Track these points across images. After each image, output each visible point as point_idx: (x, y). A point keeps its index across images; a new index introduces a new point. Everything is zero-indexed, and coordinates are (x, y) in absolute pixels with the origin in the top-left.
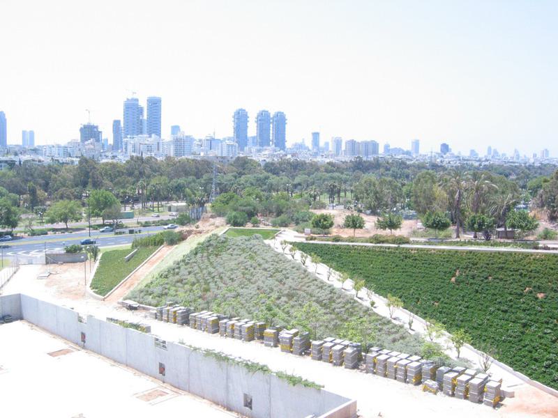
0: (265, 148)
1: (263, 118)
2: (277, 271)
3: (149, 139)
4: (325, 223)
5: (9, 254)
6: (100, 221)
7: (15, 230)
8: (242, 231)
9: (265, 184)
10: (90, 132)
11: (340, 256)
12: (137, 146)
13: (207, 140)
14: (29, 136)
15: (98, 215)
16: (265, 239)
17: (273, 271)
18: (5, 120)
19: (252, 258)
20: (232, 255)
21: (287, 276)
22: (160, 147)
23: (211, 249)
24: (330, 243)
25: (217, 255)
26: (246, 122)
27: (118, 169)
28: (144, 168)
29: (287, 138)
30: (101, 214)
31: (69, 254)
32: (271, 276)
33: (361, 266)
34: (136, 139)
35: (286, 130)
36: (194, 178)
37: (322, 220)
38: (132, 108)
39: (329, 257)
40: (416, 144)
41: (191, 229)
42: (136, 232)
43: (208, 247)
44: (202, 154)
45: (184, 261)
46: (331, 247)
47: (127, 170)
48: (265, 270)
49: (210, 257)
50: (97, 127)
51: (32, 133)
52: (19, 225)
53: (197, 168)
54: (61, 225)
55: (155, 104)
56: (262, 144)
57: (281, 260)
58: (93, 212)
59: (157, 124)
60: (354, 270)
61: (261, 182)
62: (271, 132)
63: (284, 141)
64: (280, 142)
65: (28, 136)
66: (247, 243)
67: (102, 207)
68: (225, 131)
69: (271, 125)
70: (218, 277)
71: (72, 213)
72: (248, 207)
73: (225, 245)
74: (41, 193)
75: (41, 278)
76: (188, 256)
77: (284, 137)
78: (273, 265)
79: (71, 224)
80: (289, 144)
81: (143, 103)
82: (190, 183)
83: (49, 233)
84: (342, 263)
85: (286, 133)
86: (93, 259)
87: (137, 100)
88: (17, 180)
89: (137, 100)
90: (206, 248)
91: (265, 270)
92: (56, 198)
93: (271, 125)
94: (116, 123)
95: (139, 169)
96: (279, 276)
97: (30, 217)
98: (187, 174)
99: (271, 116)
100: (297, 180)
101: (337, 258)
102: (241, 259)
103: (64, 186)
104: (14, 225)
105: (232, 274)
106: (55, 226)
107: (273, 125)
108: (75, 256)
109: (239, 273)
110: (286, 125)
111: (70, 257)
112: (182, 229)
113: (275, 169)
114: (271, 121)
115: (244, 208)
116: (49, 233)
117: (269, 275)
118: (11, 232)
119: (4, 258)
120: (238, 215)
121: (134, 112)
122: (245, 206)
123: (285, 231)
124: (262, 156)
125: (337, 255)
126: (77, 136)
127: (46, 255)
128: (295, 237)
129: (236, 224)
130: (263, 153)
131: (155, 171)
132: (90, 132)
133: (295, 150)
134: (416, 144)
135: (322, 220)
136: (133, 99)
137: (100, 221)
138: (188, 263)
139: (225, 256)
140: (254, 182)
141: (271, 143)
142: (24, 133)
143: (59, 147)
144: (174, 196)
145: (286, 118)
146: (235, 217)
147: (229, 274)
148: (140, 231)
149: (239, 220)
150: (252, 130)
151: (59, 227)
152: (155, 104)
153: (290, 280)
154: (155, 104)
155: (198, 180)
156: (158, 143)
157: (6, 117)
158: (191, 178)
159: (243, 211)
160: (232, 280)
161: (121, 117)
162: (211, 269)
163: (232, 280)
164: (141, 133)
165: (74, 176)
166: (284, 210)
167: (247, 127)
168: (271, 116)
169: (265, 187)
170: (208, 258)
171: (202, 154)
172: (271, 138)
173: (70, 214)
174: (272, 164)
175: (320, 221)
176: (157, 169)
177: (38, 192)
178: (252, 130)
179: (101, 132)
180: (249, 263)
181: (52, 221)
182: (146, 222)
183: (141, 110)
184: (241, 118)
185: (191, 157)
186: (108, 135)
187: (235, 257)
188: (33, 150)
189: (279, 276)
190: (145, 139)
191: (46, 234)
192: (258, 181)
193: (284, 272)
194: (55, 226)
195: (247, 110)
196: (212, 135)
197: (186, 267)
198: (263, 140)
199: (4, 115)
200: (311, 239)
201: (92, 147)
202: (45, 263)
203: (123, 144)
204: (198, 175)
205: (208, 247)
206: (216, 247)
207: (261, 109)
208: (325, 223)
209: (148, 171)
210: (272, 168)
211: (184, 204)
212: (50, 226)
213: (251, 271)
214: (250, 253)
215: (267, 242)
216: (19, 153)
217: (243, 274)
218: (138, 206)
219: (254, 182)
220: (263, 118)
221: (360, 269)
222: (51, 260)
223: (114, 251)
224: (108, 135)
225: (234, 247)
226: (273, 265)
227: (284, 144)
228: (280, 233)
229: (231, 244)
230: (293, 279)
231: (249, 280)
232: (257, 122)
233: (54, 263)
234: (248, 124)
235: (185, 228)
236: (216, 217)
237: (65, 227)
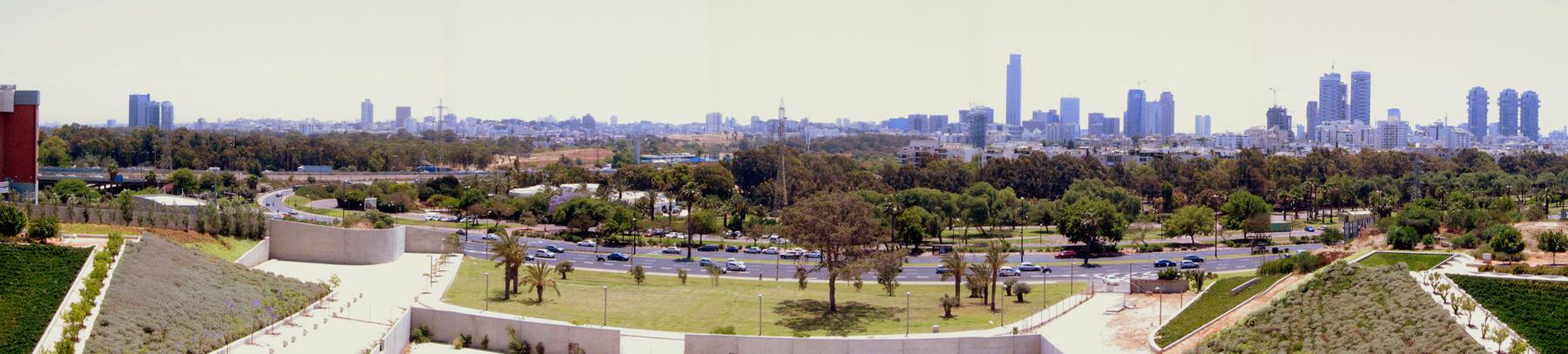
0: (1510, 137)
1: (1508, 99)
2: (1409, 322)
3: (1350, 126)
4: (1510, 245)
5: (1096, 276)
6: (1239, 235)
7: (1120, 244)
8: (1394, 257)
9: (1491, 185)
10: (1277, 117)
11: (1512, 299)
12: (1333, 135)
13: (1433, 127)
14: (1203, 122)
15: (1235, 227)
16: (1412, 270)
17: (1404, 322)
18: (1173, 102)
19: (1381, 300)
20: (1355, 295)
21: (1421, 330)
22: (1350, 139)
23: (1329, 283)
24: (1510, 276)
25: (1335, 293)
26: (1485, 104)
27: (1290, 165)
28: (1327, 163)
29: (1541, 124)
30: (1240, 225)
31: (1164, 281)
32: (1397, 331)
33: (1537, 315)
34: (1332, 127)
35: (1539, 114)
36: (1390, 177)
37: (1506, 241)
38: (1330, 86)
39: (1498, 298)
40: (367, 108)
41: (1337, 250)
42: (1282, 252)
43: (1325, 280)
44: (1417, 145)
45: (1284, 301)
46: (1503, 283)
47: (1304, 166)
48: (1393, 319)
49: (1324, 297)
50: (1284, 111)
51: (1208, 119)
52: (1125, 238)
53: (1397, 165)
54: (1186, 239)
55: (1361, 80)
56: (1506, 133)
57: (1421, 305)
58: (1229, 223)
59: (1364, 106)
60: (1527, 320)
61: (1485, 182)
62: (1519, 117)
63: (1536, 129)
64: (1531, 128)
65: (1203, 125)
66: (1384, 276)
67: (1241, 217)
68: (1457, 116)
69: (1519, 109)
70: (1320, 328)
71: (1200, 224)
72: (1422, 221)
73: (1351, 278)
74: (1177, 195)
75: (1108, 313)
76: (1292, 293)
77: (1537, 124)
78: (1407, 312)
79: (1198, 239)
80: (1544, 131)
81: (1346, 80)
82: (1384, 184)
83: (1164, 249)
84: (1513, 309)
85: (1539, 118)
86: (1196, 290)
87: (1338, 76)
88: (1153, 178)
89: (1338, 76)
90: (1323, 282)
91: (1393, 319)
92: (1197, 202)
93: (1519, 109)
94: (1311, 105)
95: (1320, 165)
96: (1409, 330)
97: (1144, 227)
98: (1381, 172)
99: (1519, 97)
100: (1540, 179)
101: (1507, 302)
102: (1366, 301)
103: (1209, 187)
104: (1118, 237)
105: (1342, 326)
106: (1176, 240)
107: (1520, 109)
108: (1174, 284)
109: (1352, 325)
110: (1539, 109)
111: (1167, 284)
112: (1325, 250)
113: (1514, 165)
114: (1519, 103)
115: (1416, 221)
116: (1164, 249)
117: (1393, 329)
118: (1113, 247)
119: (1074, 281)
120: (1403, 232)
121: (1333, 92)
122: (1418, 218)
123: (1459, 256)
124: (1497, 147)
125: (1508, 296)
126: (1262, 122)
127: (1131, 281)
128: (1468, 265)
129: (1399, 245)
130: (1507, 143)
131: (1342, 168)
132: (1277, 117)
133: (1552, 140)
134: (367, 108)
135: (1506, 241)
136: (1332, 75)
137: (1239, 235)
138: (1290, 304)
139: (1345, 295)
140: (1475, 183)
141: (1519, 131)
142: (1198, 118)
143: (1231, 135)
144: (1359, 201)
145: (1539, 99)
146: (1399, 234)
147: (1337, 324)
148: (1287, 250)
149: (1404, 239)
150: (1493, 115)
151: (1182, 242)
152: (1362, 81)
153: (1422, 338)
154: (1361, 80)
155: (1396, 180)
156: (1363, 131)
157: (1174, 99)
158: (1385, 178)
159: (1413, 225)
160: (1338, 334)
161: (1316, 98)
162: (1316, 316)
163: (1338, 334)
164: (1344, 118)
165: (1231, 173)
166: (1476, 223)
167: (1487, 110)
168: (1519, 97)
169: (1490, 189)
170: (1321, 298)
171: (1417, 145)
172: (1519, 125)
173: (1196, 225)
174: (1510, 158)
175: (1503, 241)
176: (1344, 166)
177: (1174, 194)
178: (1493, 115)
179: (1290, 117)
180: (1373, 308)
181: (1172, 234)
182: (1303, 238)
183: (1343, 89)
184: (1477, 99)
185: (1404, 149)
186: (1299, 120)
187: (1359, 297)
188: (1199, 140)
189: (1409, 330)
190: (1347, 126)
191: (1161, 250)
192: (1480, 181)
193: (1419, 325)
194: (1176, 240)
195: (1486, 89)
196: (1443, 120)
197: (1284, 310)
198: (1506, 126)
199: (1172, 96)
200: (1487, 269)
201: (1275, 136)
202: (1129, 291)
203: (1317, 132)
204: (1396, 173)
205: (1325, 280)
206: (1338, 281)
207: (1506, 88)
208: (1510, 245)
209: (1331, 167)
210: (1508, 165)
211: (1367, 212)
212: (1169, 240)
213: (1372, 321)
214: (1381, 292)
215: (1413, 274)
216: (1179, 143)
217: (1359, 325)
218: (1304, 216)
219: (1475, 183)
220: (1508, 99)
221: (1536, 319)
222: (1137, 288)
223: (1234, 278)
224: (1299, 120)
225: (1363, 282)
226: (1407, 312)
227: (1537, 133)
228: (1452, 260)
229: (1359, 276)
230: (1427, 336)
231: (1364, 335)
232: (1500, 104)
233: (1142, 292)
234: (1488, 107)
235: (1330, 249)
236: (1378, 233)
237: (1191, 242)
